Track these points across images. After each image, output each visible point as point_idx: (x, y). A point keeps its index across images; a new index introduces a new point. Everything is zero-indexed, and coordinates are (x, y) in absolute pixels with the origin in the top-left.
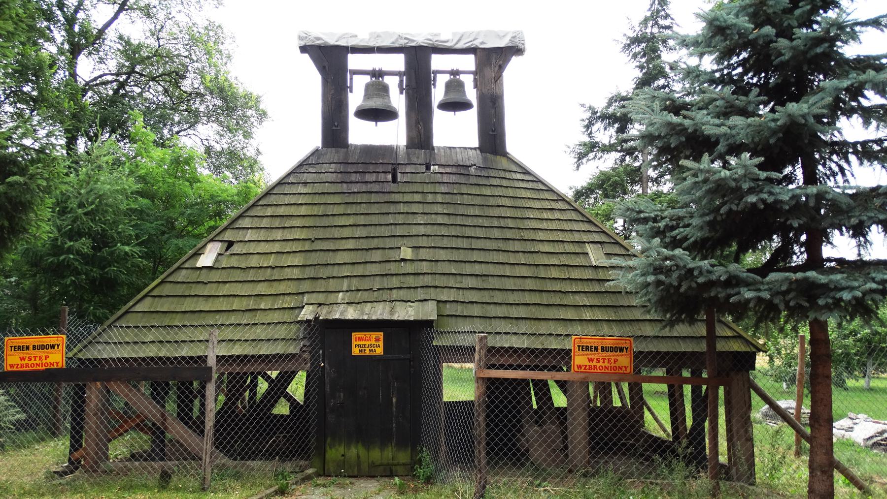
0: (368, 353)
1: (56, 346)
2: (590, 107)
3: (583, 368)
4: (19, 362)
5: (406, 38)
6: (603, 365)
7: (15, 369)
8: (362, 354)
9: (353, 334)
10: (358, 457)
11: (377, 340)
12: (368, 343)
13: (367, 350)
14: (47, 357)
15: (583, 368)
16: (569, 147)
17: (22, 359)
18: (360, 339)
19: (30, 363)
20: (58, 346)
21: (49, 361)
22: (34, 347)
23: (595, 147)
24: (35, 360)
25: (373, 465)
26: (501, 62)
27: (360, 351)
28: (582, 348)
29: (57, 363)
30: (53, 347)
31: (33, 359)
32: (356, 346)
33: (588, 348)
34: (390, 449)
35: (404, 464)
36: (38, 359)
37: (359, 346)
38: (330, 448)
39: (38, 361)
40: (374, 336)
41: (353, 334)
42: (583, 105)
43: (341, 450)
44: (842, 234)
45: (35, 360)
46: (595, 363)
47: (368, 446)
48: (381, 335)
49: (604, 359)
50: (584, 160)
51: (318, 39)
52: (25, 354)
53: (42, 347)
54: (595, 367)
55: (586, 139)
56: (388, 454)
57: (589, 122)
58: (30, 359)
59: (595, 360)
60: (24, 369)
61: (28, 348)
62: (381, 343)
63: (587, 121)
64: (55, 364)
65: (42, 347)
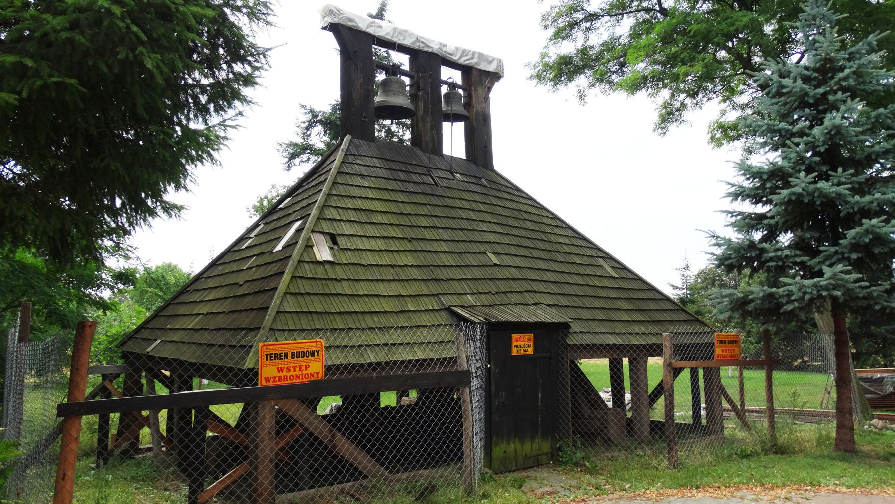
0: (522, 353)
1: (316, 353)
2: (311, 110)
3: (272, 380)
4: (277, 374)
5: (423, 42)
6: (294, 374)
7: (271, 383)
8: (518, 354)
9: (512, 335)
10: (515, 451)
11: (529, 340)
12: (522, 344)
13: (522, 351)
14: (307, 367)
15: (272, 380)
16: (281, 145)
17: (280, 370)
18: (517, 340)
19: (289, 374)
20: (318, 352)
21: (310, 371)
22: (293, 355)
23: (307, 149)
24: (295, 371)
25: (526, 458)
26: (489, 85)
27: (517, 351)
28: (271, 357)
29: (317, 374)
30: (313, 354)
31: (292, 369)
32: (515, 346)
33: (277, 357)
34: (537, 441)
35: (547, 453)
36: (297, 369)
37: (517, 346)
38: (495, 447)
39: (298, 372)
40: (526, 337)
41: (512, 335)
42: (304, 107)
43: (503, 446)
44: (708, 260)
45: (295, 371)
46: (285, 373)
47: (522, 441)
48: (531, 335)
49: (295, 367)
50: (297, 160)
51: (350, 20)
52: (284, 364)
53: (302, 355)
54: (286, 377)
55: (299, 140)
56: (529, 447)
57: (309, 125)
58: (289, 370)
59: (285, 370)
60: (283, 382)
61: (286, 356)
62: (532, 344)
63: (307, 123)
64: (316, 375)
65: (302, 355)
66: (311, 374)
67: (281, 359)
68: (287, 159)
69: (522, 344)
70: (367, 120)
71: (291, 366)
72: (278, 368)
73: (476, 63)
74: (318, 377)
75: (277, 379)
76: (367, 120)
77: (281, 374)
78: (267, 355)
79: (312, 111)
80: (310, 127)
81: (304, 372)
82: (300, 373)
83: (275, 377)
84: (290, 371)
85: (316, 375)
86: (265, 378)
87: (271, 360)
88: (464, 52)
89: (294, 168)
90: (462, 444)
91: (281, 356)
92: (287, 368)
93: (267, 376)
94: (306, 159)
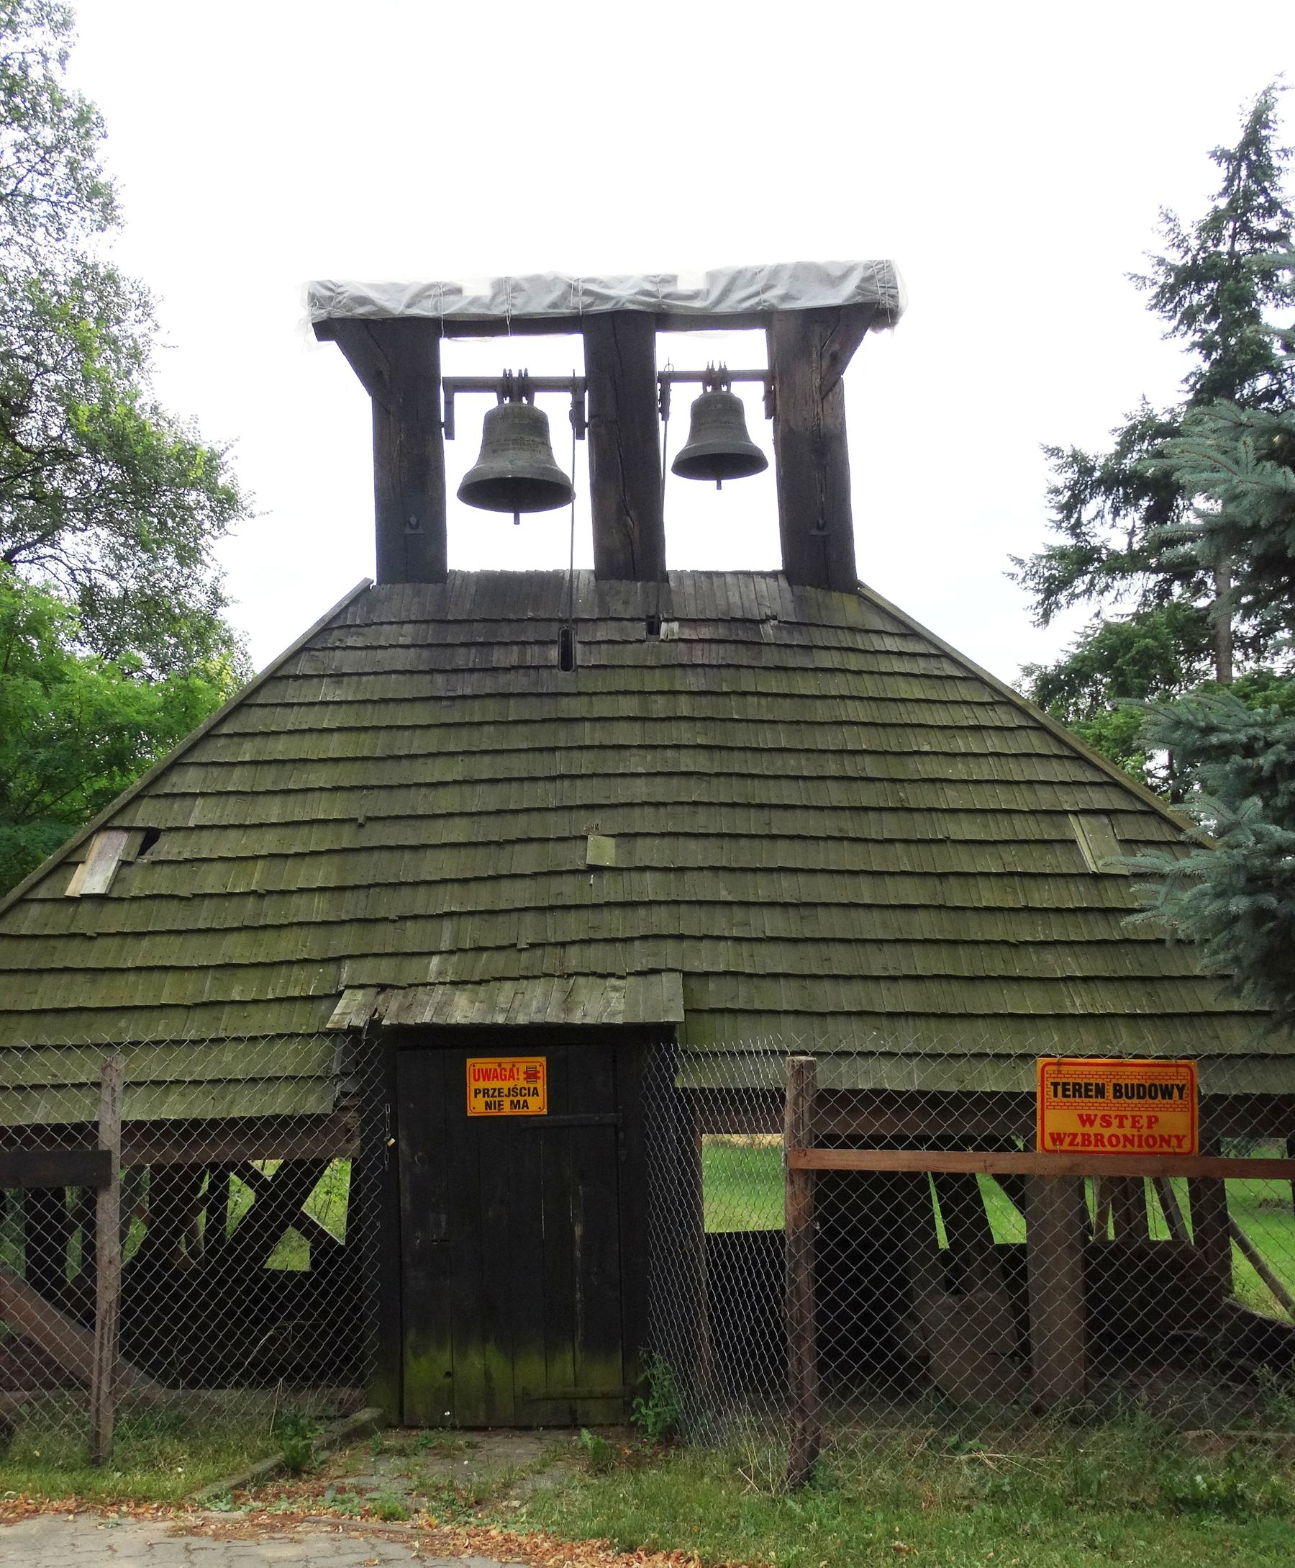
0: (507, 1110)
3: (1068, 1140)
4: (1076, 1127)
5: (587, 293)
6: (1120, 1132)
9: (470, 1061)
11: (531, 1076)
12: (506, 1085)
15: (1068, 1140)
16: (1020, 562)
17: (1086, 1120)
18: (486, 1075)
23: (1089, 560)
24: (1121, 1126)
26: (836, 347)
27: (488, 1105)
28: (1065, 1090)
29: (1180, 1139)
31: (1115, 1122)
32: (477, 1092)
36: (1128, 1123)
37: (485, 1092)
39: (1128, 1131)
40: (523, 1068)
41: (470, 1061)
42: (1055, 452)
45: (1121, 1126)
46: (1097, 1128)
48: (539, 1063)
50: (1062, 598)
55: (1065, 540)
58: (1107, 1122)
59: (1098, 1121)
61: (1100, 1091)
62: (541, 1085)
63: (1067, 494)
66: (1162, 1137)
67: (1087, 1096)
68: (1041, 596)
69: (506, 1085)
70: (420, 531)
71: (1113, 1114)
72: (1080, 1116)
73: (786, 297)
74: (1180, 1146)
75: (1079, 1139)
76: (420, 531)
77: (1087, 1129)
78: (1055, 1085)
79: (1077, 458)
80: (1071, 507)
81: (1145, 1132)
82: (1135, 1132)
83: (1075, 1136)
84: (1109, 1124)
85: (1174, 1142)
86: (1052, 1135)
87: (1064, 1096)
88: (735, 280)
89: (1058, 617)
90: (122, 1301)
91: (1087, 1090)
92: (1103, 1118)
93: (1055, 1131)
94: (1083, 587)
